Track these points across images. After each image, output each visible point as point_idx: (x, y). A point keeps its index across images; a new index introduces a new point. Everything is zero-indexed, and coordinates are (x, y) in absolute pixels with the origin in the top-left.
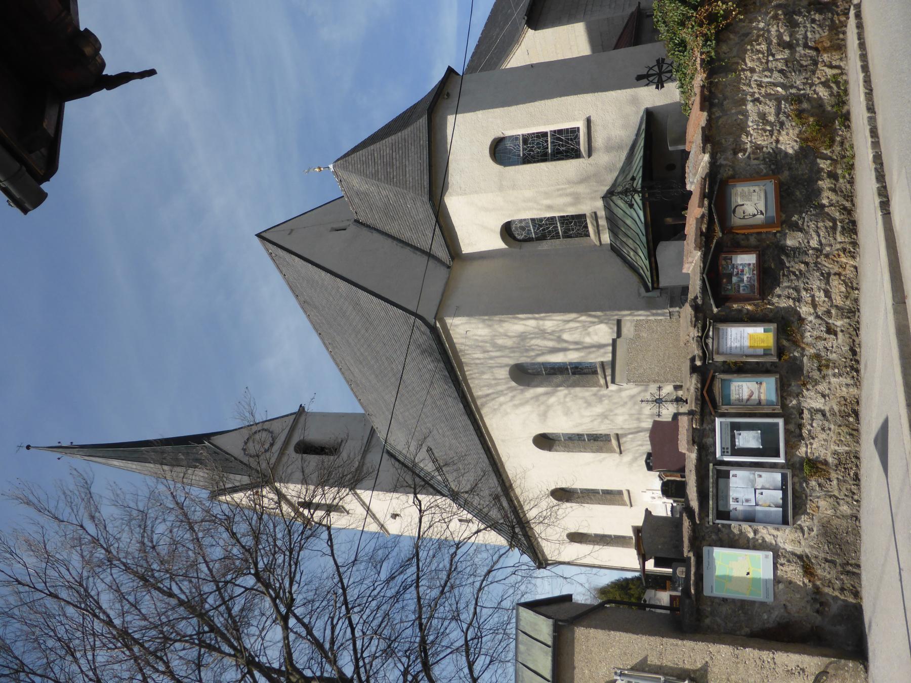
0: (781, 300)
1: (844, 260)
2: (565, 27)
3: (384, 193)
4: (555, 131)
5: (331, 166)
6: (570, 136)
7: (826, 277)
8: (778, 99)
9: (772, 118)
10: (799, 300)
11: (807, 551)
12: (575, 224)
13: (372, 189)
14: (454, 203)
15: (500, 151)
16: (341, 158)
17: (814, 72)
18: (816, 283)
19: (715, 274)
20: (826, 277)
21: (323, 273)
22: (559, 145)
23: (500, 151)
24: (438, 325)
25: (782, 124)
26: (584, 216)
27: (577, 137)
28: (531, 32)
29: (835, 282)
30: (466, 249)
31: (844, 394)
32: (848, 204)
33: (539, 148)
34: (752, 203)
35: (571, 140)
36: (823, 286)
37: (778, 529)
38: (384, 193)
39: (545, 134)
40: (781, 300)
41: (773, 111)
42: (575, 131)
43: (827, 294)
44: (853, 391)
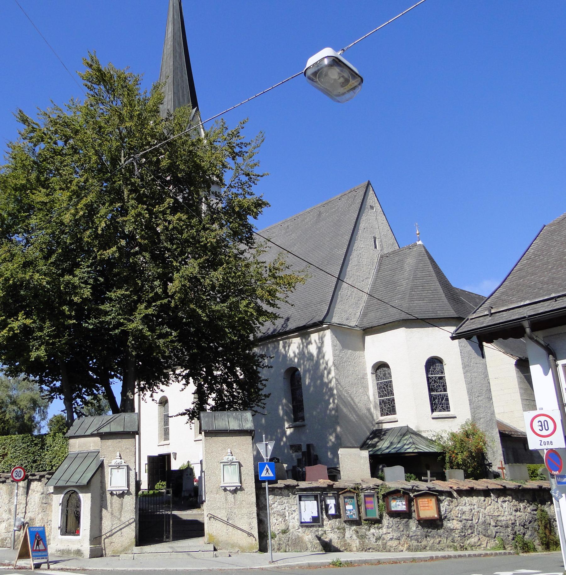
0: (386, 520)
1: (406, 546)
2: (517, 386)
3: (404, 283)
4: (447, 396)
5: (420, 243)
6: (445, 406)
7: (398, 539)
9: (464, 517)
10: (388, 527)
11: (291, 531)
12: (389, 408)
13: (406, 274)
14: (401, 333)
15: (434, 364)
16: (427, 252)
17: (485, 535)
18: (396, 535)
19: (395, 494)
20: (398, 539)
21: (348, 238)
23: (434, 364)
24: (324, 326)
25: (461, 521)
26: (395, 414)
27: (444, 410)
28: (514, 361)
29: (396, 542)
30: (368, 338)
31: (353, 545)
32: (428, 548)
33: (437, 387)
34: (427, 509)
35: (442, 407)
36: (394, 537)
37: (298, 519)
38: (404, 283)
39: (445, 390)
40: (386, 520)
41: (467, 518)
42: (447, 409)
43: (392, 539)
44: (355, 549)
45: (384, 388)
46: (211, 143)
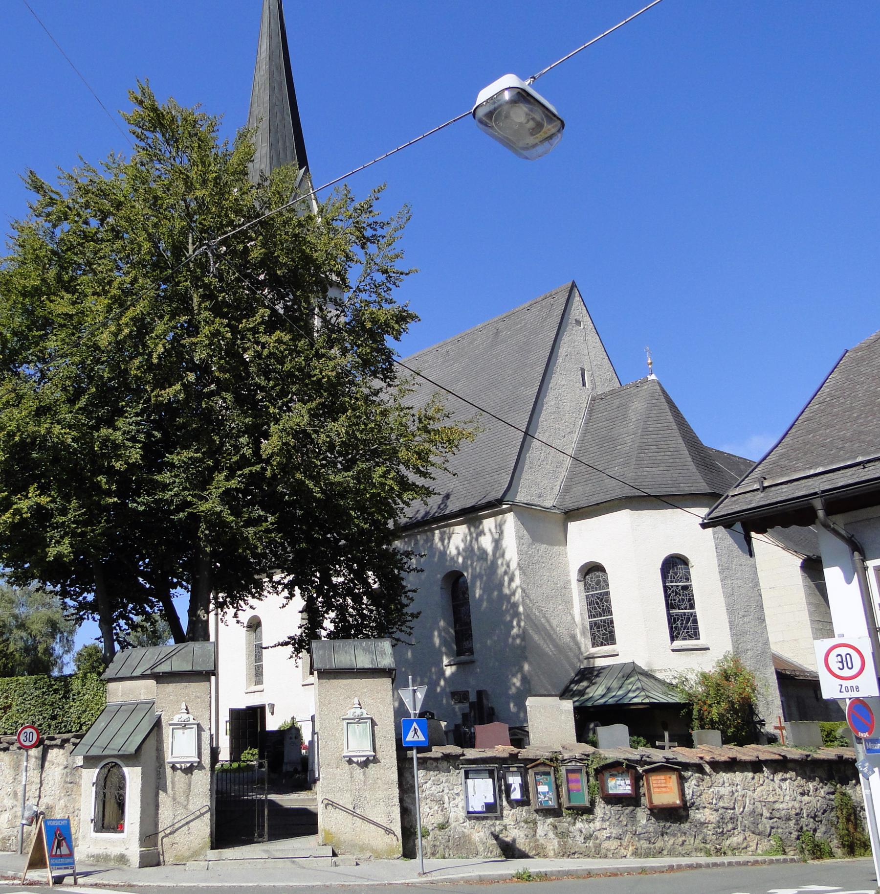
0: (601, 808)
1: (631, 849)
2: (804, 601)
3: (628, 440)
4: (695, 616)
5: (653, 377)
6: (691, 632)
7: (619, 838)
8: (784, 745)
9: (721, 804)
10: (603, 820)
11: (453, 826)
12: (604, 634)
13: (631, 426)
14: (624, 517)
15: (674, 565)
16: (664, 392)
17: (753, 833)
18: (615, 831)
19: (615, 767)
20: (619, 838)
21: (541, 369)
22: (682, 620)
23: (674, 565)
24: (504, 506)
25: (717, 810)
26: (614, 643)
27: (691, 637)
28: (799, 562)
29: (616, 843)
30: (572, 526)
31: (548, 848)
32: (665, 852)
33: (679, 601)
35: (688, 632)
36: (613, 835)
37: (463, 807)
38: (628, 440)
39: (692, 607)
40: (601, 808)
41: (726, 805)
42: (696, 635)
43: (609, 838)
44: (551, 853)
45: (597, 603)
46: (328, 223)
